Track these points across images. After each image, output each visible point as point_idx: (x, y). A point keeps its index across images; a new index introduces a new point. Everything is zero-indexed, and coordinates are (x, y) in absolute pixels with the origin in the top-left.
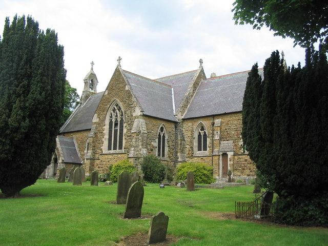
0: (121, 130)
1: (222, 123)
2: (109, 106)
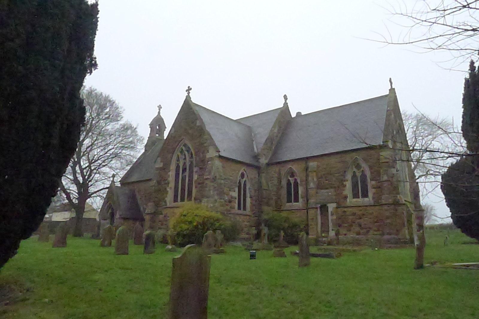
0: (191, 177)
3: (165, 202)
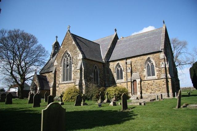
0: (71, 68)
2: (63, 55)
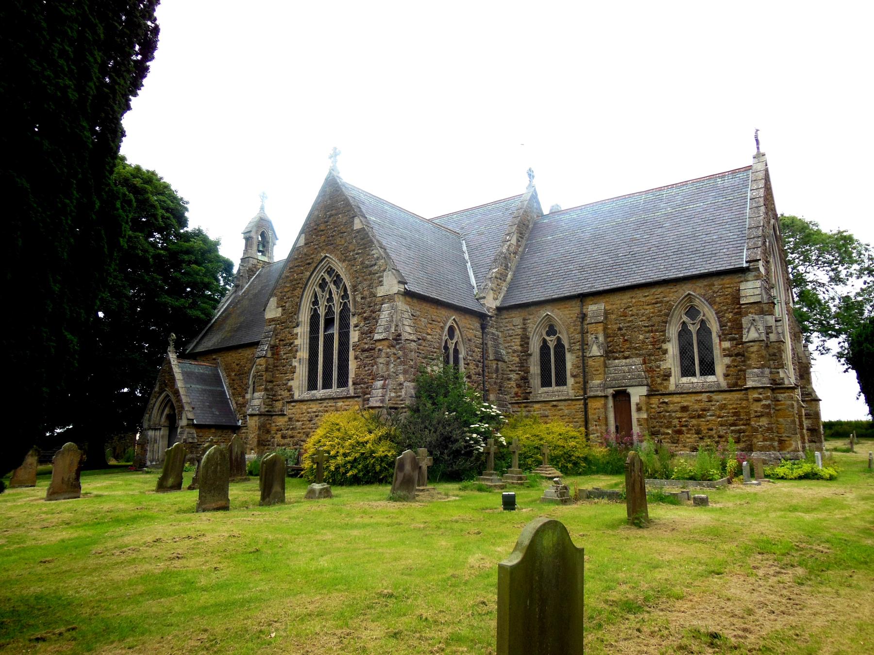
1: (606, 313)
2: (308, 274)
3: (290, 389)
